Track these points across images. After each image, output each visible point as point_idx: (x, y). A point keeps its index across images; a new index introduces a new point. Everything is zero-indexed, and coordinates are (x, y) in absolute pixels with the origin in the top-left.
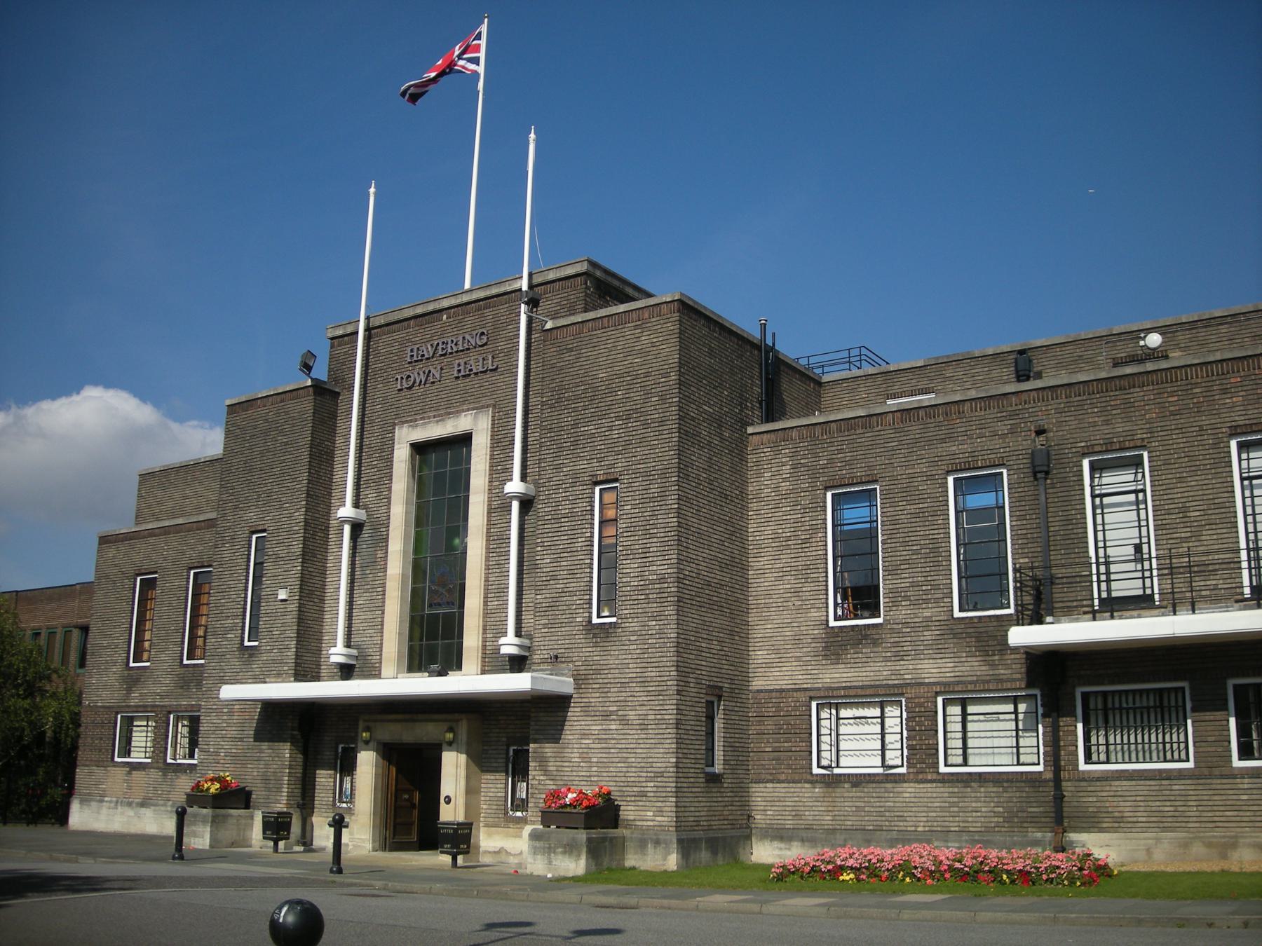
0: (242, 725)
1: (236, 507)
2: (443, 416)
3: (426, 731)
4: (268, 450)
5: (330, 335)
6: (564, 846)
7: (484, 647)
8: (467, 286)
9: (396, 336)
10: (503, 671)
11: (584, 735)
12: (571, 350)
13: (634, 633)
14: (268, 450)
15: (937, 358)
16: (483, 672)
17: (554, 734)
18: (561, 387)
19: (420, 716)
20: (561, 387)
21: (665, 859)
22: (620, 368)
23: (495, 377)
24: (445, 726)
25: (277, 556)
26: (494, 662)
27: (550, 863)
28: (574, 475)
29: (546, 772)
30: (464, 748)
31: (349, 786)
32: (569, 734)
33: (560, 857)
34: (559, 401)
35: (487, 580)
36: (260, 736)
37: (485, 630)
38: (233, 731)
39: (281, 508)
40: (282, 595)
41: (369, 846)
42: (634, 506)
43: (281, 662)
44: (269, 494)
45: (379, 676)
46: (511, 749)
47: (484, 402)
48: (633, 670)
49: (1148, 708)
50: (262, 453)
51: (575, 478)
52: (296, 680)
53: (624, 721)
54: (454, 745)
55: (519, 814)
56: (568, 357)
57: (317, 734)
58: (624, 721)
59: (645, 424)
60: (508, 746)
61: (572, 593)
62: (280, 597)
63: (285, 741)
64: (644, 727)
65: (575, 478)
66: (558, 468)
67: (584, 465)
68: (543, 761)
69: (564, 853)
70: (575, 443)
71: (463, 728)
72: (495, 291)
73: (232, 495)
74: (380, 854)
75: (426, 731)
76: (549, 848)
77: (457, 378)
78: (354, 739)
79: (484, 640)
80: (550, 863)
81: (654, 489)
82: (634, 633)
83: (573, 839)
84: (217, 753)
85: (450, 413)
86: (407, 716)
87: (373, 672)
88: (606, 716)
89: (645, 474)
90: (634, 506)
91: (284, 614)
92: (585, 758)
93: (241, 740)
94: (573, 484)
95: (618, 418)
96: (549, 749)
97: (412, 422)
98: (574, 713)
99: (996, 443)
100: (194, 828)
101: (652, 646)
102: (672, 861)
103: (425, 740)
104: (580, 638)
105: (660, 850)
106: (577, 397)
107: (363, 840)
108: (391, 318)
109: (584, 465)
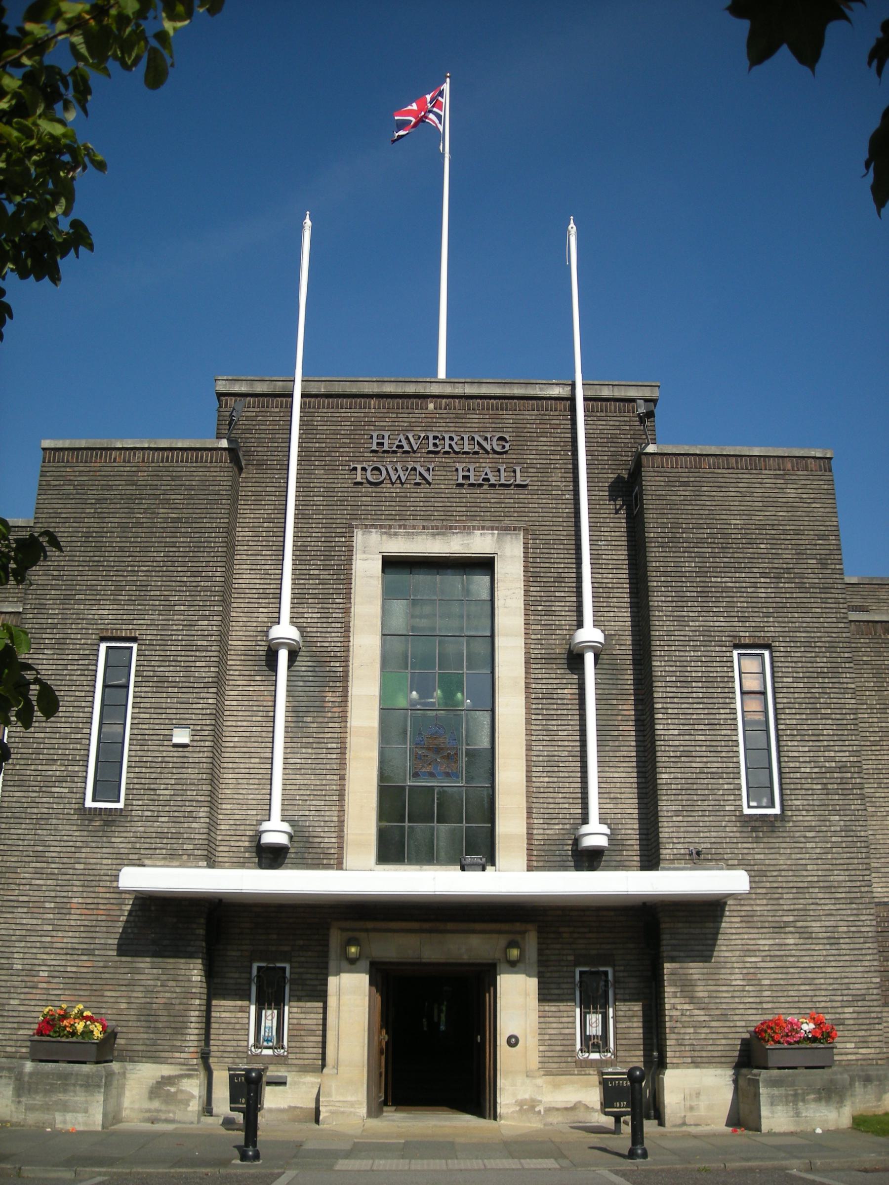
1: (67, 597)
2: (445, 525)
4: (139, 524)
5: (221, 387)
6: (818, 1092)
7: (530, 835)
8: (442, 374)
9: (345, 413)
10: (565, 868)
12: (686, 484)
13: (810, 828)
14: (139, 524)
15: (872, 578)
16: (530, 868)
17: (703, 947)
18: (676, 525)
19: (450, 926)
20: (676, 525)
21: (879, 1099)
22: (758, 518)
23: (523, 495)
24: (503, 941)
26: (541, 858)
27: (798, 1114)
28: (706, 632)
30: (535, 969)
32: (724, 950)
33: (813, 1106)
34: (673, 540)
35: (529, 748)
37: (529, 813)
38: (69, 939)
39: (169, 608)
40: (181, 736)
41: (363, 1111)
42: (796, 680)
43: (178, 836)
44: (143, 587)
45: (339, 865)
46: (255, 966)
47: (507, 522)
48: (813, 873)
50: (123, 527)
51: (708, 636)
53: (806, 934)
54: (520, 965)
55: (595, 1056)
56: (687, 491)
57: (259, 950)
58: (806, 934)
59: (801, 587)
60: (251, 962)
62: (176, 740)
63: (191, 956)
64: (833, 941)
65: (708, 636)
66: (681, 621)
67: (721, 622)
68: (687, 987)
69: (819, 1100)
70: (704, 594)
71: (531, 942)
74: (375, 1124)
76: (795, 1095)
77: (460, 485)
78: (324, 955)
79: (530, 827)
80: (798, 1114)
81: (822, 663)
82: (810, 828)
83: (831, 1081)
84: (31, 972)
85: (451, 528)
86: (426, 926)
88: (779, 928)
89: (808, 644)
90: (796, 680)
91: (182, 765)
92: (752, 978)
93: (90, 952)
94: (706, 643)
95: (763, 575)
96: (695, 970)
97: (387, 530)
98: (729, 924)
100: (62, 1096)
101: (836, 845)
103: (465, 958)
104: (732, 830)
105: (871, 1088)
106: (700, 542)
107: (352, 1104)
108: (338, 388)
109: (721, 622)
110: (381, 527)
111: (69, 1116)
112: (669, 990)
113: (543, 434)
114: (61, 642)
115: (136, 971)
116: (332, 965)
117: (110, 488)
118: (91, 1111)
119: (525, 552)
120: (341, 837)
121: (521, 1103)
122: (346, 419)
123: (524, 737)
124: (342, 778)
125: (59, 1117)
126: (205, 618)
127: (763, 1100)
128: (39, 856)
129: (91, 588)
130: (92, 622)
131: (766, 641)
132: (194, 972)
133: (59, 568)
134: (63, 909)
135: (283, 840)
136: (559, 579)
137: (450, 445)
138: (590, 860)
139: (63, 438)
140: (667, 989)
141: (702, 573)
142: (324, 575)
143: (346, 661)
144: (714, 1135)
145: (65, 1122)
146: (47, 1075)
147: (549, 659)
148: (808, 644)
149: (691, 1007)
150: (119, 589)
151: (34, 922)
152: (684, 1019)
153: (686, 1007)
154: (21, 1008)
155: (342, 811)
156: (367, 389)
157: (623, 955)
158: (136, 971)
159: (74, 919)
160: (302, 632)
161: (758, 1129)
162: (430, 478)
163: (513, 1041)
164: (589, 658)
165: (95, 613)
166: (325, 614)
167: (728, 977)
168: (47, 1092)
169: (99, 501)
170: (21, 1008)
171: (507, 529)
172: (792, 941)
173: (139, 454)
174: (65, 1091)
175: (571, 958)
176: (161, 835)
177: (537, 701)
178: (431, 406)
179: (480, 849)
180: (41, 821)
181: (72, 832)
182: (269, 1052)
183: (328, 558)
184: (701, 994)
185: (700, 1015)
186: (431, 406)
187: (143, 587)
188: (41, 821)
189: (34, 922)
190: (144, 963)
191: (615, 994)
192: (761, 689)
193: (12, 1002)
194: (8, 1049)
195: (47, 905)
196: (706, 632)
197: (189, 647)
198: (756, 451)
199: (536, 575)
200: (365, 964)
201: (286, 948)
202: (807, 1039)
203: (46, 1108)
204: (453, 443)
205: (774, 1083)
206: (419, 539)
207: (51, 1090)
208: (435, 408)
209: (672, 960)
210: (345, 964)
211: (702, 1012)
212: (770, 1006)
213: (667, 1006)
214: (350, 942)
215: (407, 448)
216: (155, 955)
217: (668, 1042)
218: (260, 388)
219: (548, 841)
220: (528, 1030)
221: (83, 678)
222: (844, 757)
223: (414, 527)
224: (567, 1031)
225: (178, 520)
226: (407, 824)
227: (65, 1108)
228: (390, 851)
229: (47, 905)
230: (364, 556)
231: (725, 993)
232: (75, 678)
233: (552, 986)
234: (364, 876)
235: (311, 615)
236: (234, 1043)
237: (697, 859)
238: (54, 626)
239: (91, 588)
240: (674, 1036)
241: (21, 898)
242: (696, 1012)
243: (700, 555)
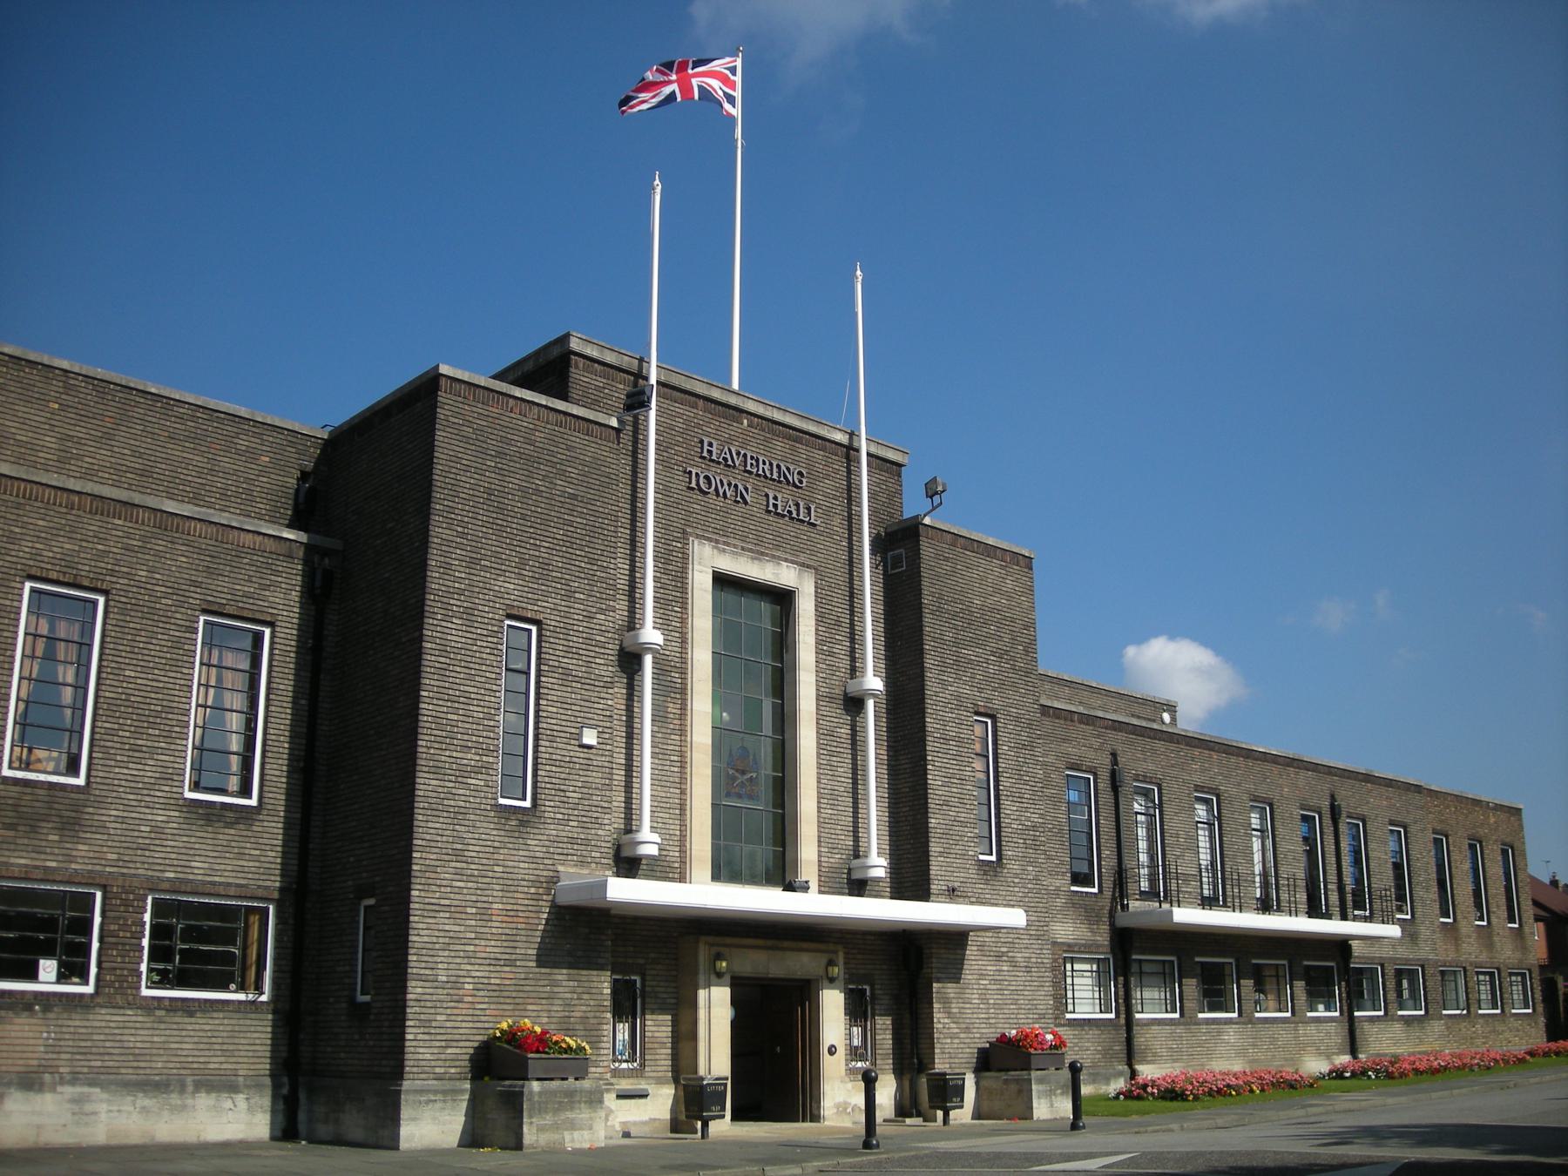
0: (511, 938)
1: (473, 562)
3: (800, 964)
4: (538, 492)
11: (982, 976)
19: (786, 944)
25: (567, 673)
29: (949, 1014)
31: (619, 1036)
32: (968, 975)
36: (546, 958)
38: (492, 948)
39: (569, 595)
43: (586, 842)
45: (682, 879)
47: (802, 558)
49: (1495, 976)
52: (851, 894)
53: (1013, 963)
56: (947, 566)
58: (1013, 963)
61: (963, 824)
62: (586, 741)
63: (601, 968)
68: (946, 1002)
72: (812, 428)
73: (463, 535)
75: (800, 964)
84: (456, 984)
85: (762, 554)
86: (769, 943)
87: (680, 875)
89: (1017, 719)
91: (587, 767)
96: (951, 989)
99: (1091, 754)
100: (569, 1115)
102: (242, 1119)
110: (717, 542)
111: (576, 1134)
115: (555, 984)
116: (702, 978)
117: (509, 442)
118: (595, 1127)
120: (682, 851)
121: (837, 1106)
123: (815, 770)
124: (683, 792)
127: (1034, 1094)
128: (458, 855)
129: (496, 555)
130: (499, 595)
131: (539, 617)
134: (484, 915)
136: (838, 623)
138: (859, 887)
139: (463, 368)
141: (956, 644)
143: (683, 673)
144: (963, 1125)
145: (573, 1141)
146: (554, 1093)
147: (831, 698)
148: (1017, 719)
150: (523, 563)
151: (457, 928)
154: (448, 1024)
155: (683, 826)
156: (701, 389)
157: (901, 972)
158: (555, 984)
159: (496, 926)
161: (396, 1148)
162: (748, 498)
163: (832, 1051)
164: (648, 660)
165: (501, 585)
168: (556, 1111)
169: (500, 454)
170: (448, 1024)
173: (536, 410)
174: (572, 1109)
176: (572, 841)
177: (824, 734)
180: (459, 814)
181: (488, 830)
182: (624, 1065)
187: (545, 565)
188: (459, 814)
189: (457, 928)
190: (561, 975)
191: (643, 1004)
192: (525, 668)
194: (438, 1070)
195: (469, 910)
196: (958, 697)
198: (991, 541)
200: (727, 978)
201: (641, 961)
202: (1051, 1047)
203: (556, 1127)
205: (1041, 1081)
206: (742, 560)
207: (560, 1108)
209: (938, 981)
210: (713, 977)
214: (719, 957)
216: (571, 966)
218: (610, 358)
219: (834, 870)
222: (1036, 819)
225: (574, 497)
227: (573, 1126)
228: (724, 870)
229: (469, 910)
234: (703, 893)
237: (952, 894)
238: (461, 592)
239: (496, 555)
241: (443, 902)
243: (955, 627)
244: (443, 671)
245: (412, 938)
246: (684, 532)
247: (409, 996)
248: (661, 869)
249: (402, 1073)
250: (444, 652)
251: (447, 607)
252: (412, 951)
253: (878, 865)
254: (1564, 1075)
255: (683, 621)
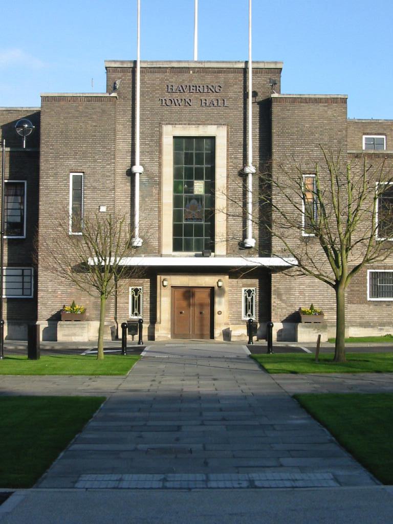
22: (316, 124)
29: (281, 300)
39: (95, 161)
62: (101, 207)
70: (293, 155)
84: (54, 292)
92: (301, 293)
112: (273, 296)
113: (236, 84)
114: (56, 174)
119: (228, 134)
122: (158, 78)
124: (159, 221)
125: (73, 337)
126: (109, 164)
132: (228, 277)
133: (52, 145)
135: (140, 245)
137: (199, 90)
140: (272, 296)
142: (151, 144)
149: (280, 302)
150: (76, 153)
152: (278, 306)
153: (279, 302)
154: (52, 304)
160: (144, 168)
161: (57, 341)
163: (220, 313)
165: (67, 163)
166: (152, 159)
167: (294, 292)
170: (52, 304)
171: (221, 124)
172: (317, 281)
175: (241, 285)
178: (191, 72)
179: (209, 248)
183: (152, 136)
184: (284, 298)
185: (283, 305)
186: (191, 72)
187: (84, 153)
193: (49, 302)
197: (104, 176)
199: (231, 143)
204: (200, 89)
208: (193, 73)
211: (284, 304)
212: (308, 302)
213: (272, 302)
215: (182, 91)
217: (272, 314)
220: (342, 370)
221: (65, 188)
223: (185, 124)
224: (239, 310)
226: (183, 237)
230: (166, 136)
231: (292, 299)
232: (62, 188)
233: (234, 295)
235: (147, 160)
236: (124, 314)
238: (53, 168)
240: (274, 312)
242: (282, 304)
243: (292, 139)
244: (47, 195)
245: (39, 279)
246: (160, 123)
247: (39, 296)
248: (147, 249)
249: (37, 319)
250: (47, 189)
251: (47, 174)
252: (39, 283)
253: (251, 242)
254: (391, 299)
255: (160, 158)
